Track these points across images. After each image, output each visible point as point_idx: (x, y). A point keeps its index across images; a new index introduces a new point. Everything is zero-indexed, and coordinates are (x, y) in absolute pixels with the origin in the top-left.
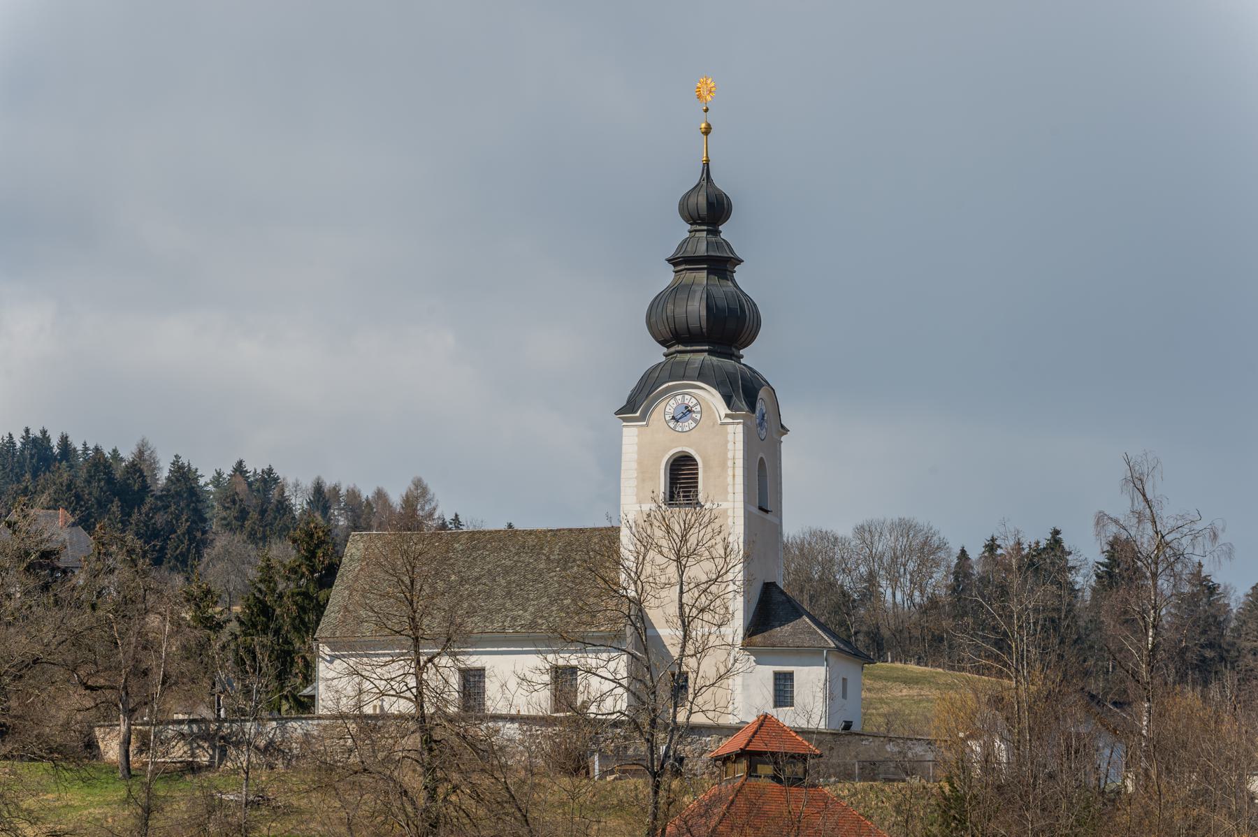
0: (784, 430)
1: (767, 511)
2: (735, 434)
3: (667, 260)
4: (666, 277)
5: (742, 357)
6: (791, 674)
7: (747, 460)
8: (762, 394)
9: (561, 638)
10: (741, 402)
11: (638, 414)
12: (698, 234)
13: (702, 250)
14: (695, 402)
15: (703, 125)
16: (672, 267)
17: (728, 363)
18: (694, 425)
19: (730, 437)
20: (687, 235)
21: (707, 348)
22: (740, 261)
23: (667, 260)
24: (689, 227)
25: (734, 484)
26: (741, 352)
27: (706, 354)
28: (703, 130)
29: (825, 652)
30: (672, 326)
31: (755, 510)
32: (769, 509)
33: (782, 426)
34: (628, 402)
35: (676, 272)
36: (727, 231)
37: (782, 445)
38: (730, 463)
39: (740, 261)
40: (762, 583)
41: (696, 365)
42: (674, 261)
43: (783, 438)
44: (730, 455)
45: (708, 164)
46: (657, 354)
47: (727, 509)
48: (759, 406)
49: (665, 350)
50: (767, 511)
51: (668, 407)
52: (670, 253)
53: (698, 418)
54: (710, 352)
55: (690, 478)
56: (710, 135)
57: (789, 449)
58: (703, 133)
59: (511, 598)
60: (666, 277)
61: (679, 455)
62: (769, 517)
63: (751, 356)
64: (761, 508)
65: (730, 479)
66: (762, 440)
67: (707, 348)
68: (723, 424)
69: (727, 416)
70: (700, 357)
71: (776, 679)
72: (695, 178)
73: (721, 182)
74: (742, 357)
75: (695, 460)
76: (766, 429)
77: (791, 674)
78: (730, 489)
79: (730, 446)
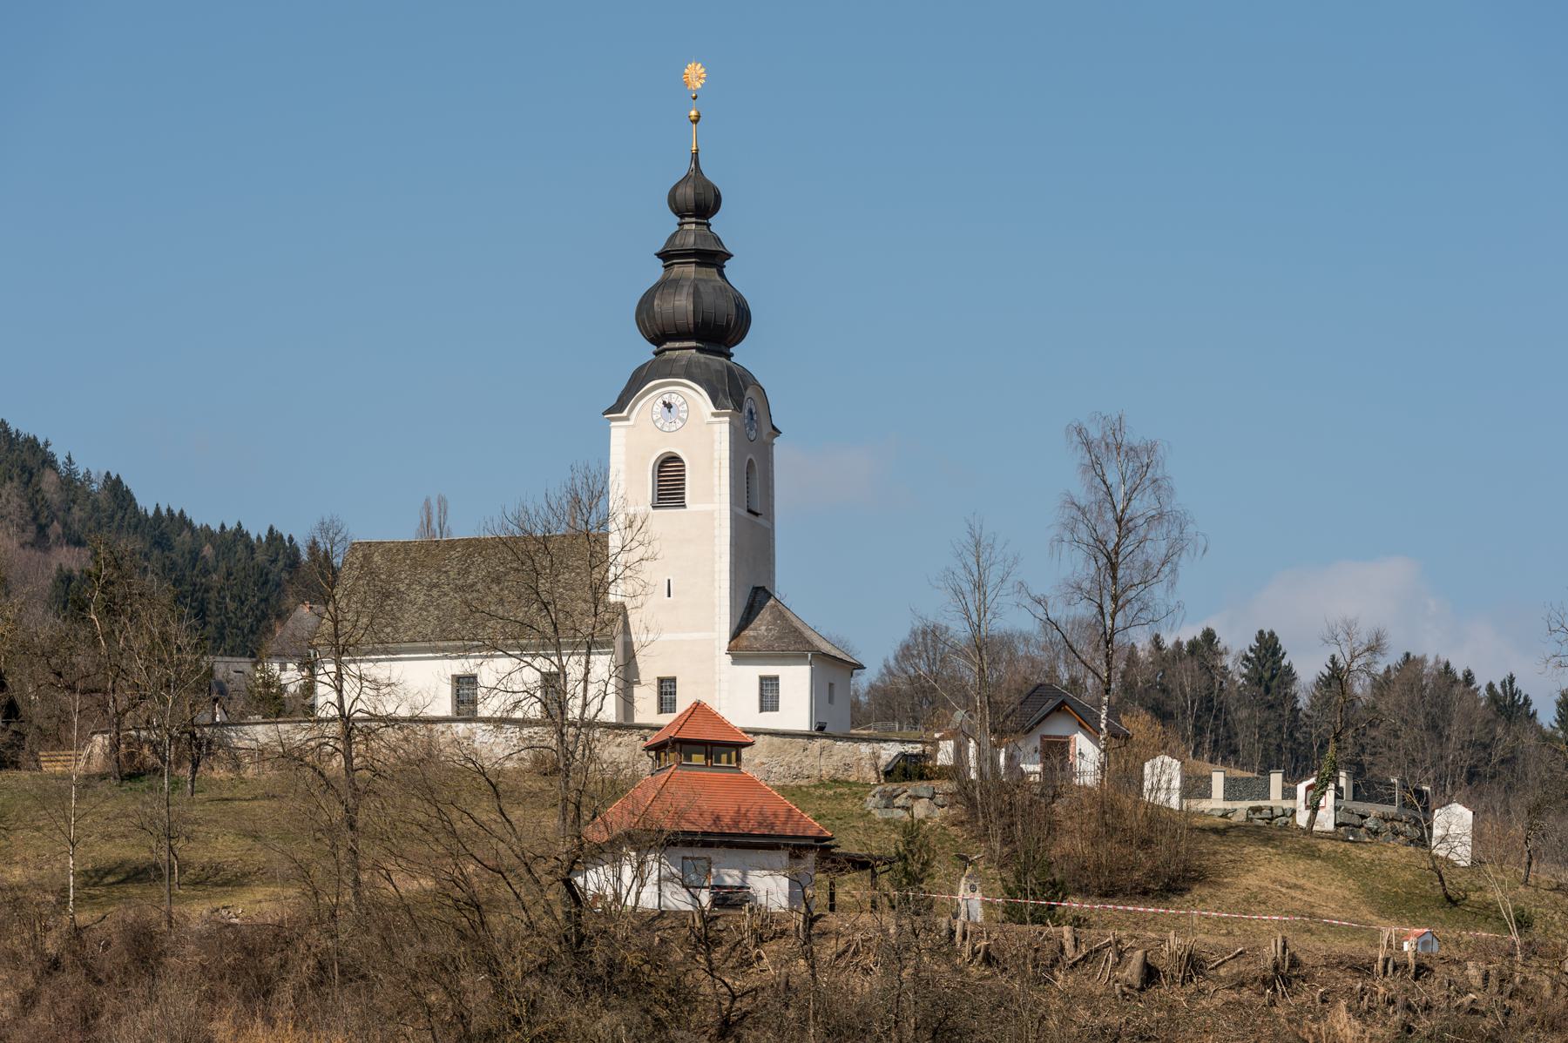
1: (756, 514)
2: (721, 430)
3: (656, 254)
4: (655, 271)
5: (732, 355)
6: (777, 678)
7: (735, 581)
8: (749, 393)
9: (553, 643)
10: (727, 399)
11: (625, 414)
12: (686, 227)
13: (690, 242)
14: (682, 400)
15: (693, 113)
16: (661, 262)
17: (717, 361)
18: (681, 424)
19: (716, 437)
20: (677, 228)
21: (694, 260)
22: (729, 256)
23: (656, 254)
24: (678, 220)
25: (720, 623)
26: (732, 350)
27: (694, 351)
28: (692, 118)
29: (809, 655)
30: (661, 328)
31: (744, 513)
32: (758, 512)
33: (774, 427)
34: (618, 401)
35: (665, 267)
36: (717, 223)
37: (774, 447)
38: (716, 464)
39: (729, 256)
40: (751, 588)
42: (659, 255)
43: (776, 440)
44: (716, 455)
45: (697, 154)
46: (647, 351)
47: (714, 511)
48: (747, 405)
49: (655, 348)
50: (756, 514)
51: (656, 406)
52: (659, 249)
53: (685, 417)
54: (698, 349)
55: (679, 489)
56: (699, 123)
57: (781, 450)
58: (692, 121)
59: (503, 605)
60: (657, 271)
61: (667, 456)
62: (759, 520)
63: (743, 354)
64: (750, 511)
66: (752, 441)
67: (694, 260)
68: (709, 423)
69: (714, 415)
70: (686, 351)
71: (761, 684)
72: (683, 168)
73: (710, 174)
74: (732, 355)
75: (682, 461)
76: (756, 431)
77: (777, 678)
78: (716, 491)
79: (717, 446)
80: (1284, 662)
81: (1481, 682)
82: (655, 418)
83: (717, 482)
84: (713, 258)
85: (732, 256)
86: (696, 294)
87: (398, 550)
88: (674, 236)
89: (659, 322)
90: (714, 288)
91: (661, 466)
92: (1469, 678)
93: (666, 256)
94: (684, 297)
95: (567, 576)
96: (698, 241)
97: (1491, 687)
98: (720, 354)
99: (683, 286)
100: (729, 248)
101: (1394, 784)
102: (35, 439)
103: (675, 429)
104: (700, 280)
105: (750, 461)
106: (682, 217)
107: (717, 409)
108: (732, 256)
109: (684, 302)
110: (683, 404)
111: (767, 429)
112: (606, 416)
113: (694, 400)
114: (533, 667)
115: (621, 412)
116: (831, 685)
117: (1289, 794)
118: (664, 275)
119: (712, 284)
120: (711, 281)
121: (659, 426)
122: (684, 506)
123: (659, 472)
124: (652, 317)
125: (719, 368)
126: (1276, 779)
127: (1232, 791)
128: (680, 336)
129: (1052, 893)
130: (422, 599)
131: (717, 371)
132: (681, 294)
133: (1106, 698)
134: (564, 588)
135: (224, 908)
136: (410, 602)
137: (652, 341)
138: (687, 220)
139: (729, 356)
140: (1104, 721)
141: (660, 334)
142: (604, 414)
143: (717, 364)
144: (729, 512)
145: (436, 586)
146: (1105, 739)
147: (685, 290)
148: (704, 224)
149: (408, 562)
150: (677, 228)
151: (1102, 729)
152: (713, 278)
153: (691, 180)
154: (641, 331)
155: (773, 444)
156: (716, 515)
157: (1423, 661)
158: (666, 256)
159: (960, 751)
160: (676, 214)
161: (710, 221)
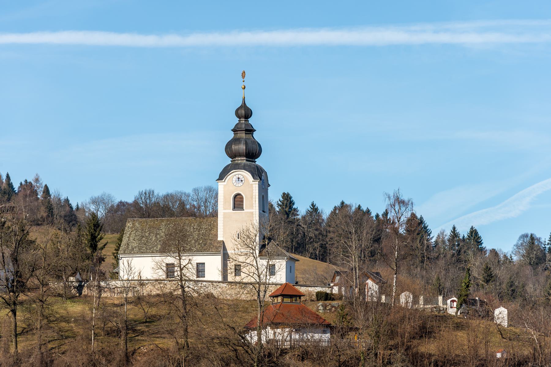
0: (269, 185)
1: (264, 212)
5: (256, 162)
11: (223, 180)
12: (241, 122)
16: (233, 133)
19: (254, 188)
20: (238, 122)
24: (238, 119)
26: (256, 160)
32: (265, 211)
33: (269, 184)
36: (251, 121)
38: (254, 197)
41: (242, 165)
44: (254, 194)
45: (244, 99)
46: (229, 161)
51: (233, 178)
52: (233, 128)
60: (231, 135)
63: (259, 162)
65: (254, 202)
74: (256, 162)
79: (254, 191)
80: (294, 207)
81: (373, 214)
82: (233, 182)
83: (254, 202)
84: (250, 131)
85: (256, 130)
86: (246, 144)
87: (144, 222)
88: (237, 124)
89: (234, 152)
90: (251, 141)
91: (235, 197)
92: (368, 212)
93: (234, 130)
94: (242, 145)
95: (203, 231)
96: (246, 127)
97: (377, 216)
98: (253, 161)
99: (241, 141)
100: (255, 128)
101: (477, 300)
102: (67, 201)
103: (240, 186)
104: (247, 139)
105: (263, 195)
106: (240, 118)
107: (254, 179)
108: (256, 130)
109: (242, 147)
110: (243, 178)
111: (266, 185)
112: (217, 181)
113: (247, 175)
114: (253, 277)
115: (222, 180)
116: (291, 267)
117: (445, 303)
118: (234, 136)
119: (251, 140)
120: (250, 139)
121: (235, 185)
122: (244, 210)
123: (234, 199)
124: (231, 150)
125: (254, 167)
126: (440, 298)
127: (426, 302)
128: (240, 156)
129: (92, 274)
130: (154, 238)
131: (253, 168)
132: (241, 143)
133: (395, 276)
134: (202, 235)
135: (142, 346)
136: (150, 239)
137: (231, 157)
138: (242, 119)
139: (255, 162)
140: (395, 283)
141: (232, 155)
142: (216, 181)
143: (253, 165)
144: (258, 212)
145: (158, 234)
146: (395, 289)
147: (242, 142)
148: (247, 121)
149: (148, 226)
150: (238, 122)
151: (394, 286)
152: (251, 138)
153: (243, 107)
154: (227, 155)
155: (268, 189)
156: (254, 213)
157: (350, 206)
158: (234, 130)
159: (340, 289)
160: (238, 118)
161: (249, 120)
